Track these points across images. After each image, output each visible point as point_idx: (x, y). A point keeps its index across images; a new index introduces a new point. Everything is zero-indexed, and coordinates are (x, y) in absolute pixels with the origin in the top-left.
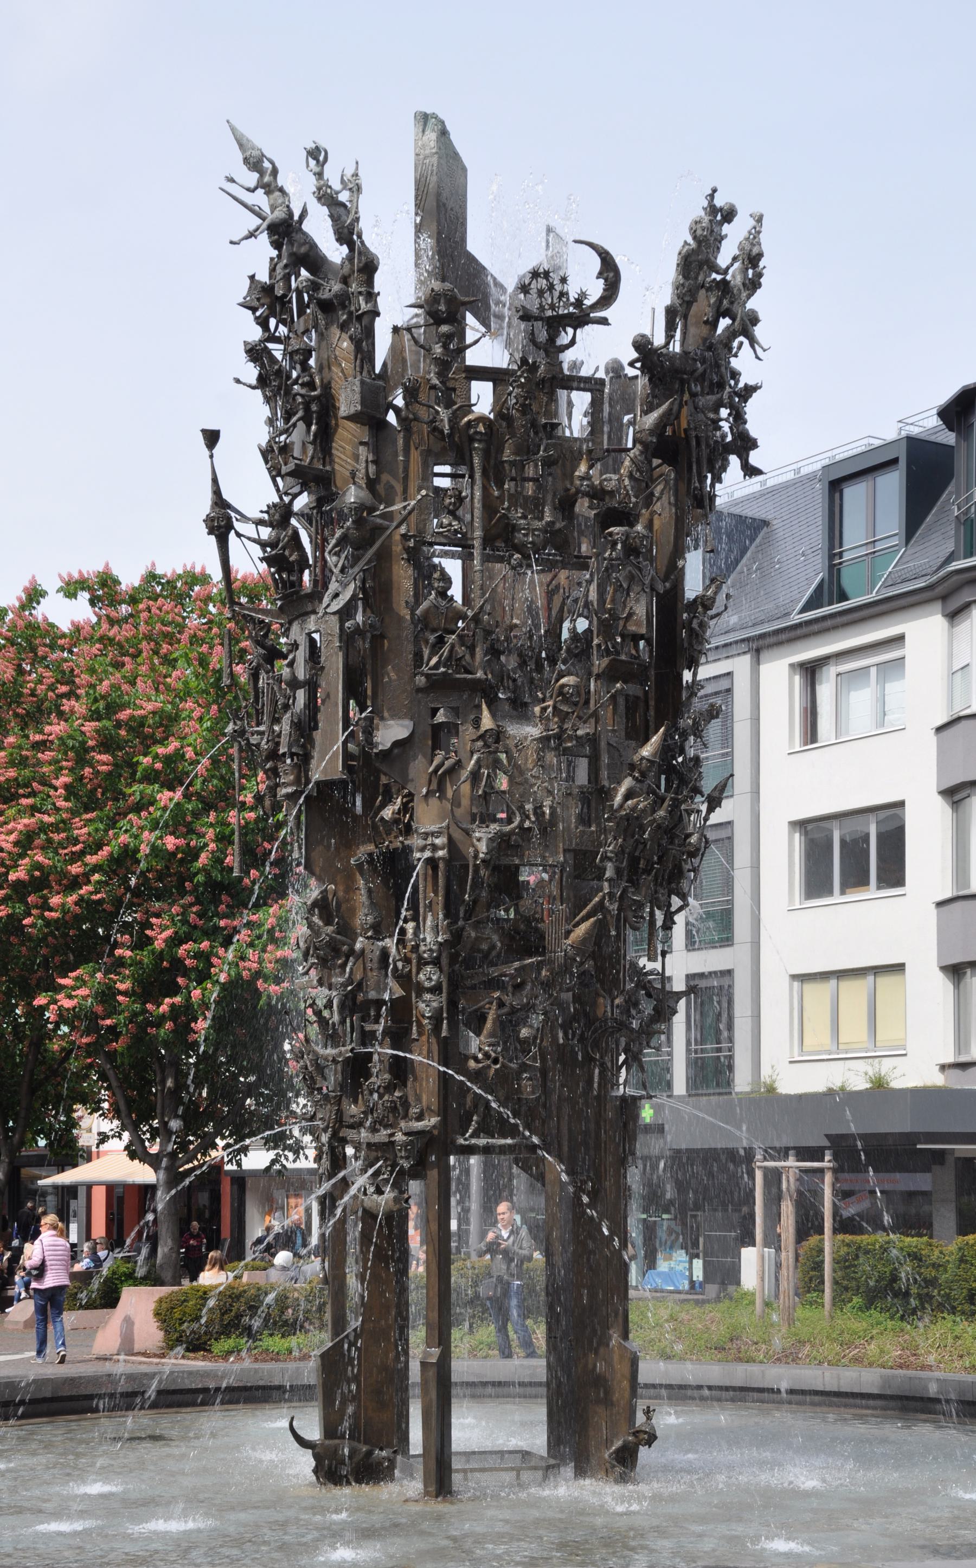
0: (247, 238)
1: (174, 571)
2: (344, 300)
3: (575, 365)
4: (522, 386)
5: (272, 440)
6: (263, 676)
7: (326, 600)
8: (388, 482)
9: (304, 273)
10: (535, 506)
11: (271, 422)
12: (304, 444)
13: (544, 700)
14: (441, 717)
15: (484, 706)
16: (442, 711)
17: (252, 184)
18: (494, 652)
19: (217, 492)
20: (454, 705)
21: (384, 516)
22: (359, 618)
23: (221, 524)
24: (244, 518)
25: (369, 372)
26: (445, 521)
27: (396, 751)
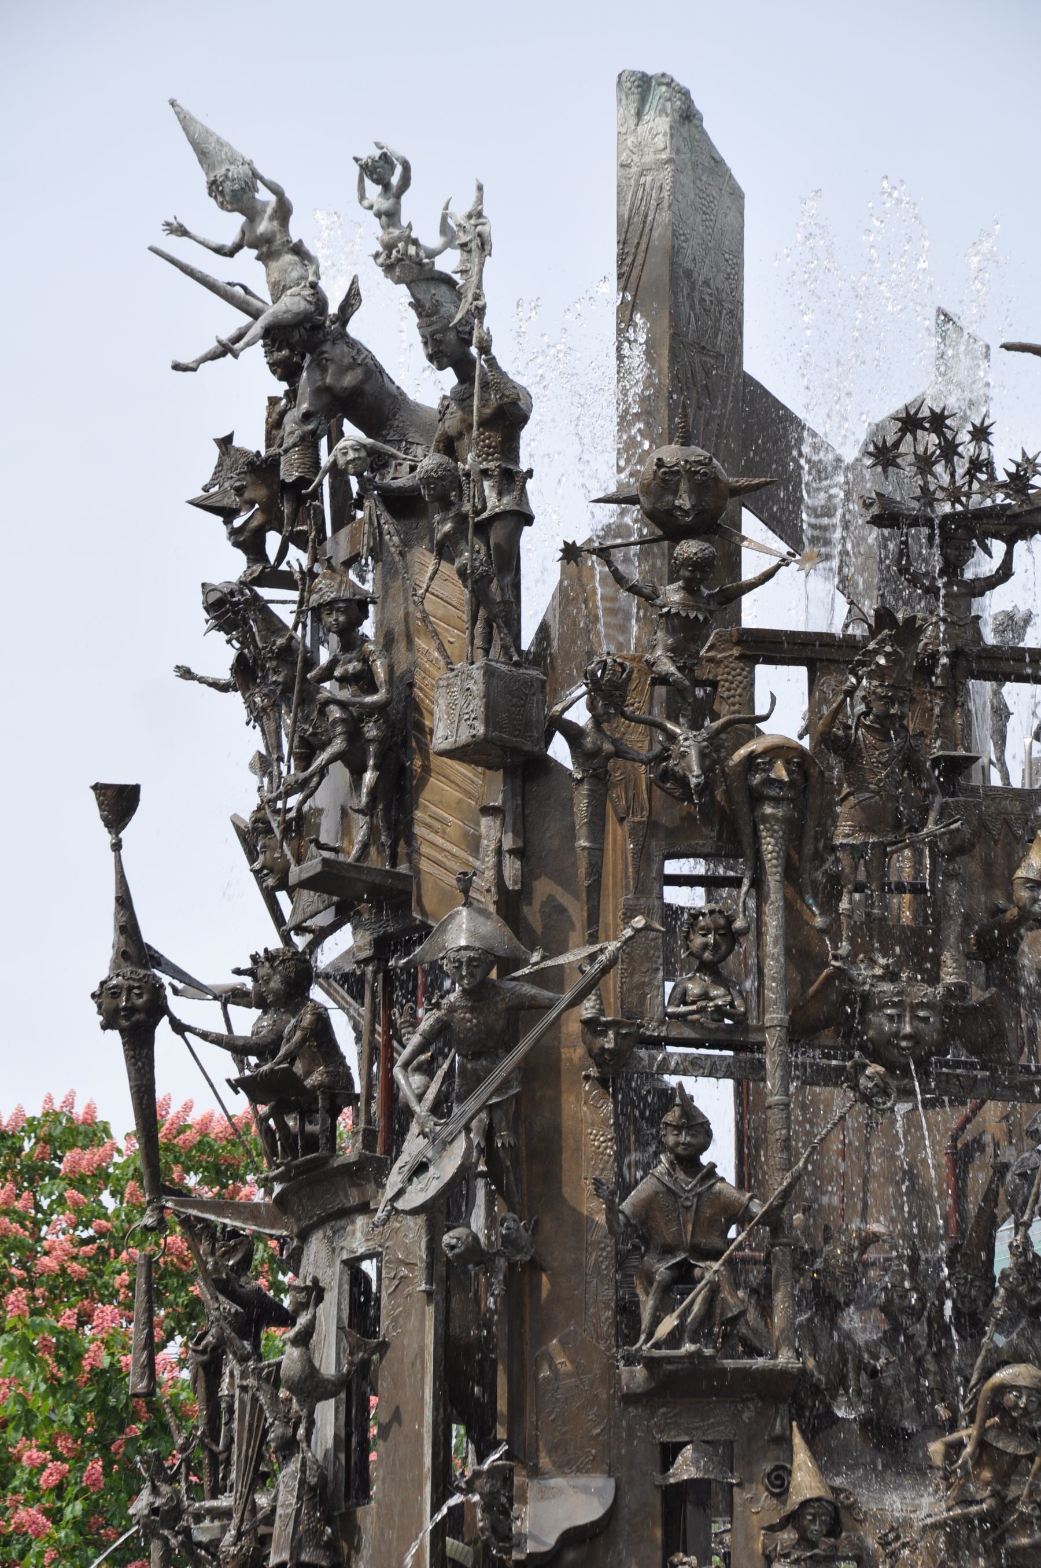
0: (213, 356)
1: (20, 1112)
2: (446, 488)
3: (1014, 623)
4: (879, 673)
5: (267, 804)
6: (231, 1366)
7: (394, 1180)
8: (551, 898)
9: (350, 430)
10: (919, 951)
11: (264, 764)
12: (344, 813)
13: (953, 1425)
14: (686, 1467)
15: (798, 1440)
16: (688, 1451)
17: (229, 239)
18: (825, 1303)
19: (128, 926)
20: (722, 1433)
21: (539, 978)
22: (478, 1221)
23: (136, 1001)
24: (195, 988)
25: (505, 648)
26: (694, 989)
27: (570, 1556)
